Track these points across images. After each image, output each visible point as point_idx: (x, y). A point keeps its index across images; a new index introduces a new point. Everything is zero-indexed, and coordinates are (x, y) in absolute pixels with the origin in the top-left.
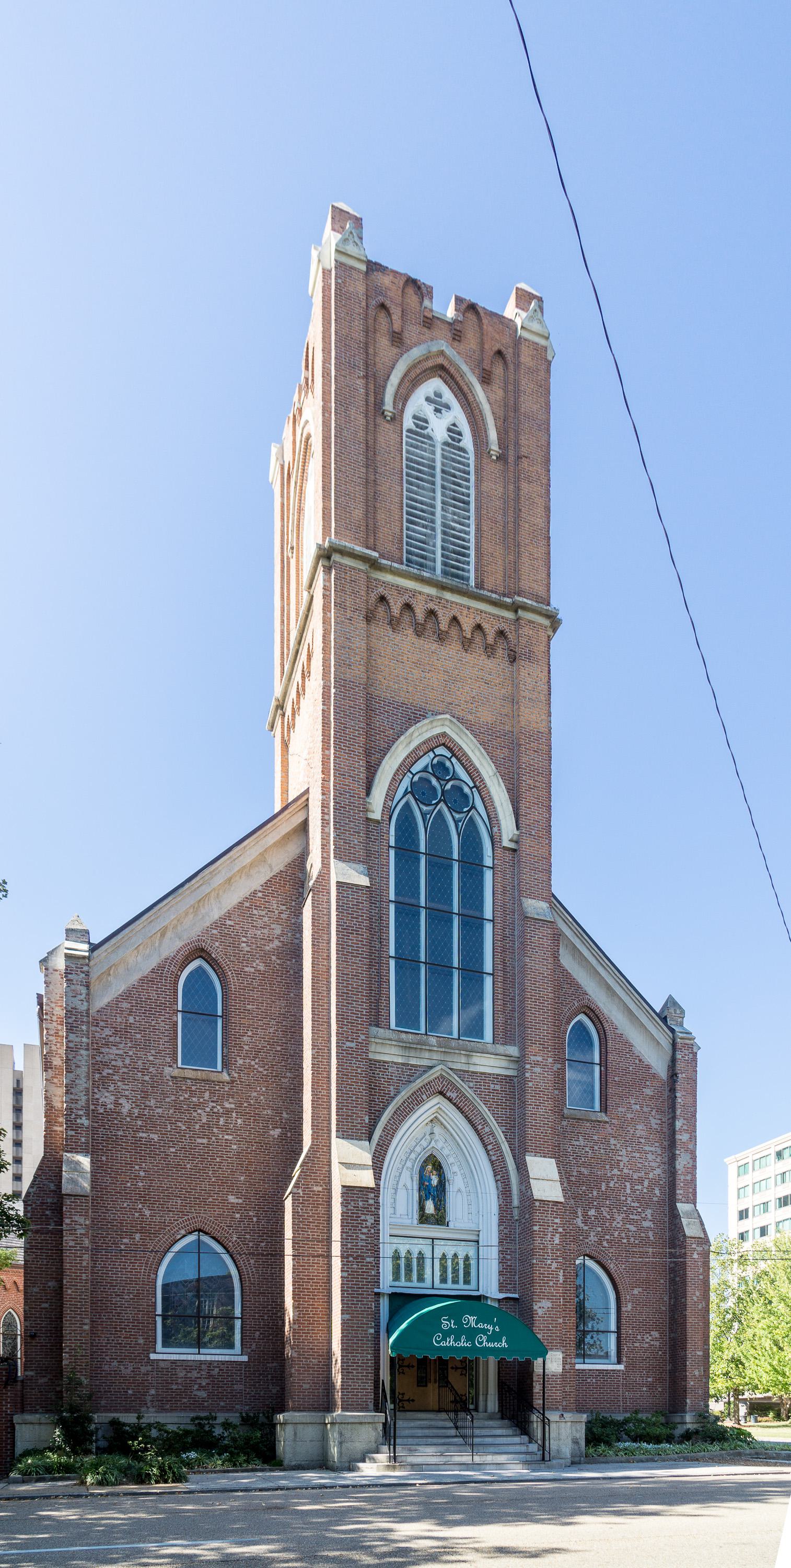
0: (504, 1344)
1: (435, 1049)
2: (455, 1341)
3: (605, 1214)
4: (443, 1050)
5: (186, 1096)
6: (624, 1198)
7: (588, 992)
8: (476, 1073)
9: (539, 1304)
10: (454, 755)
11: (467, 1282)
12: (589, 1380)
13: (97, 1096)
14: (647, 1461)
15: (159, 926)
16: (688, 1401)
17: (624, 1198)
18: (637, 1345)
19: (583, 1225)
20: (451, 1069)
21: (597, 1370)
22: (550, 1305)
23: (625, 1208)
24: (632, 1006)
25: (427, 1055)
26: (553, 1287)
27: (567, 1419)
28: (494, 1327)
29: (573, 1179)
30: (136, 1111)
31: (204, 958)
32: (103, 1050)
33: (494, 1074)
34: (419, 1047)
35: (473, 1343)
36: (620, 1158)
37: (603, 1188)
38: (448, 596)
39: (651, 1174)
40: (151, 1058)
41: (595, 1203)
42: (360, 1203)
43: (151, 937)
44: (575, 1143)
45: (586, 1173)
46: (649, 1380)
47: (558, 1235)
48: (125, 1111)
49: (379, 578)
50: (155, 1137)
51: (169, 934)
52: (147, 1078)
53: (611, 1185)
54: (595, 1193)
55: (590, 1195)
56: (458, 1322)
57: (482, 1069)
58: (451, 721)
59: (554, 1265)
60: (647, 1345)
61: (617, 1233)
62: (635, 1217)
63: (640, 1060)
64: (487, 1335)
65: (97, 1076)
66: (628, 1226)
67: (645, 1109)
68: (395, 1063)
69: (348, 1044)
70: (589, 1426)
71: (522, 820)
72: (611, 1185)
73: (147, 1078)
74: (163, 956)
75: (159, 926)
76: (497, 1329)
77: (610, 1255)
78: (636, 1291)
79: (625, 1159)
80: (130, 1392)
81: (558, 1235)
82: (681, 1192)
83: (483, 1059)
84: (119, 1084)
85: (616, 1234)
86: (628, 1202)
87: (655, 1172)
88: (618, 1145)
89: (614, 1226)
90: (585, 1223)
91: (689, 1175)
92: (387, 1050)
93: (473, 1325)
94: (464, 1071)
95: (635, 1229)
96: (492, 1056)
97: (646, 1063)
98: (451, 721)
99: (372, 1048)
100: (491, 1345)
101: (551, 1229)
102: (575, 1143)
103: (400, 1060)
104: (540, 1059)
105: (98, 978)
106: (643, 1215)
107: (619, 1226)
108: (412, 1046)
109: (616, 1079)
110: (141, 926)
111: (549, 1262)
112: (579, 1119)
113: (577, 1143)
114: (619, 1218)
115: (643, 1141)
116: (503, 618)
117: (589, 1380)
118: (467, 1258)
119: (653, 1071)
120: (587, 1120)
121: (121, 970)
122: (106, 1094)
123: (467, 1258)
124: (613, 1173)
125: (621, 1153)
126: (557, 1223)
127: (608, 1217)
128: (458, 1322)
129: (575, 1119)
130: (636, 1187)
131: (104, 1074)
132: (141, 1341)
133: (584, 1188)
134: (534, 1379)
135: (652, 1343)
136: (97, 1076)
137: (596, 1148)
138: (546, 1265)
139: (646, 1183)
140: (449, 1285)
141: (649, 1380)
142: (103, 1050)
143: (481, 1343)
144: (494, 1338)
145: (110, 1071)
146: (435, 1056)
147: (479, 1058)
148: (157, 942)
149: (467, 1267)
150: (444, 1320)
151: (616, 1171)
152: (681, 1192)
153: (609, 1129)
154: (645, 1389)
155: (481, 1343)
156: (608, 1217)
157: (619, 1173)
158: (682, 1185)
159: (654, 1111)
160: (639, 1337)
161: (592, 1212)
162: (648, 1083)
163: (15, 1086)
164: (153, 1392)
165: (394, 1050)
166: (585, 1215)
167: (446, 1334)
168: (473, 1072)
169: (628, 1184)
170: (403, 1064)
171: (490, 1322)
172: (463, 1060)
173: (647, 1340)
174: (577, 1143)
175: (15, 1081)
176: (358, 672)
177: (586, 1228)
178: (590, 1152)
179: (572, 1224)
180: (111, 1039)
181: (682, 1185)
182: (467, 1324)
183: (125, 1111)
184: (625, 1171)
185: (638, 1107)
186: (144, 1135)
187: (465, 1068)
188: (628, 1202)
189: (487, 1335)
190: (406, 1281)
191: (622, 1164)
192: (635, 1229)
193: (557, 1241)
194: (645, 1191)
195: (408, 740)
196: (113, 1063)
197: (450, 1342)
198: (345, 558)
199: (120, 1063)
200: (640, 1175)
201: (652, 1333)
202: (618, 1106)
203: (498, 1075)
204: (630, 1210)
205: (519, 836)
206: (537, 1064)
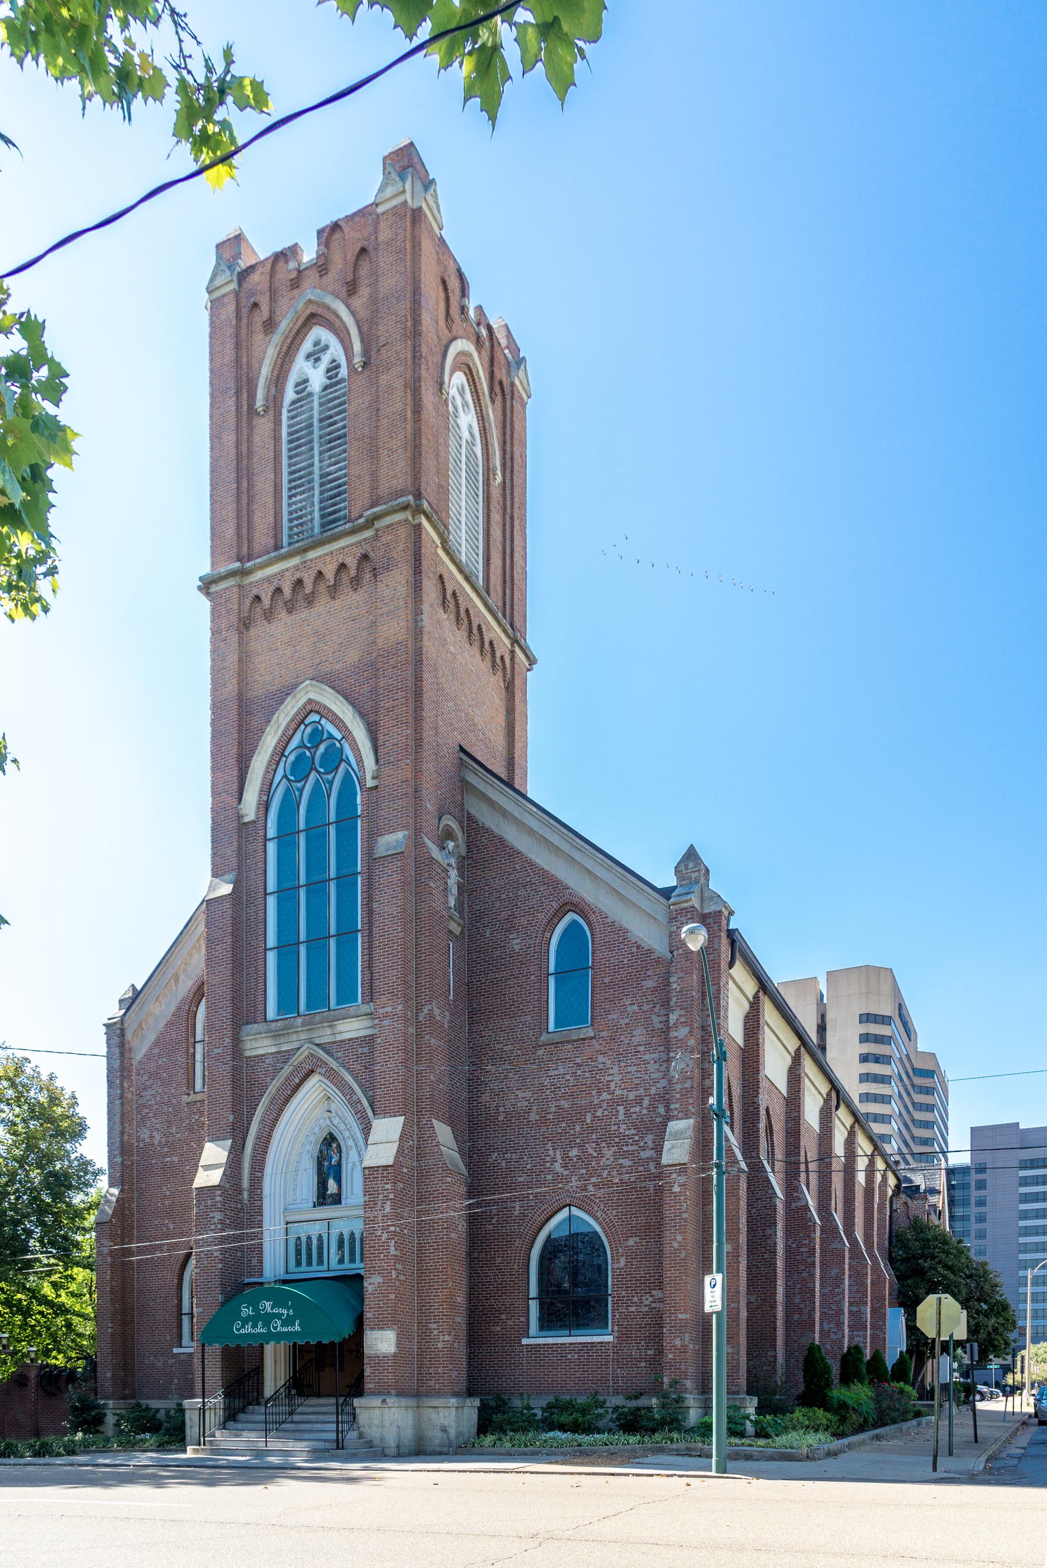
0: (297, 1328)
1: (300, 1029)
2: (252, 1327)
3: (591, 1151)
4: (307, 1028)
5: (197, 1117)
6: (616, 1127)
7: (569, 885)
8: (344, 1041)
9: (370, 1281)
10: (302, 722)
11: (320, 1262)
12: (569, 1356)
13: (139, 1134)
14: (533, 1454)
15: (171, 972)
16: (665, 1379)
17: (616, 1127)
18: (633, 1309)
19: (562, 1169)
20: (318, 1045)
21: (579, 1343)
22: (380, 1280)
23: (617, 1140)
24: (617, 884)
25: (294, 1037)
26: (384, 1259)
27: (390, 1405)
28: (288, 1311)
29: (550, 1116)
30: (163, 1140)
31: (574, 911)
32: (142, 1094)
33: (361, 1037)
34: (285, 1032)
35: (269, 1329)
36: (610, 1078)
37: (588, 1121)
38: (311, 555)
39: (654, 1088)
40: (173, 1091)
41: (578, 1141)
42: (209, 1202)
43: (166, 986)
44: (553, 1073)
45: (566, 1106)
46: (650, 1352)
47: (388, 1202)
48: (156, 1142)
49: (252, 580)
50: (175, 1159)
51: (182, 977)
52: (170, 1109)
53: (599, 1114)
54: (578, 1128)
55: (572, 1132)
56: (256, 1309)
57: (348, 1036)
58: (311, 685)
59: (385, 1236)
60: (647, 1309)
61: (606, 1172)
62: (631, 1148)
63: (638, 947)
64: (282, 1319)
65: (139, 1116)
66: (621, 1161)
67: (646, 1008)
68: (271, 1054)
69: (216, 1051)
70: (482, 1410)
71: (381, 750)
72: (599, 1114)
73: (170, 1109)
74: (179, 999)
75: (171, 972)
76: (291, 1312)
77: (597, 1200)
78: (631, 1242)
79: (617, 1078)
80: (161, 1382)
81: (388, 1202)
82: (677, 1106)
83: (346, 1025)
84: (153, 1119)
85: (605, 1173)
86: (622, 1131)
87: (658, 1085)
88: (609, 1062)
89: (602, 1164)
90: (565, 1166)
91: (689, 1081)
92: (321, 1032)
93: (269, 1310)
94: (333, 1043)
95: (630, 1163)
96: (354, 1019)
97: (646, 948)
98: (311, 685)
99: (248, 1045)
100: (285, 1329)
101: (381, 1197)
102: (553, 1073)
103: (273, 1050)
104: (389, 1009)
105: (133, 1035)
106: (642, 1144)
107: (608, 1163)
108: (279, 1033)
109: (606, 980)
110: (156, 981)
111: (379, 1233)
112: (558, 1043)
113: (556, 1072)
114: (609, 1153)
115: (641, 1049)
116: (365, 540)
117: (569, 1356)
118: (320, 1237)
119: (657, 955)
120: (568, 1042)
121: (151, 1021)
122: (145, 1131)
123: (320, 1237)
124: (601, 1098)
125: (611, 1072)
126: (388, 1190)
127: (595, 1154)
128: (256, 1309)
129: (552, 1044)
130: (632, 1110)
131: (144, 1114)
132: (168, 1338)
133: (564, 1125)
134: (365, 1361)
135: (653, 1305)
136: (139, 1116)
137: (579, 1072)
138: (376, 1236)
139: (646, 1102)
140: (304, 1267)
141: (650, 1352)
142: (142, 1094)
143: (275, 1328)
144: (288, 1322)
145: (147, 1111)
146: (303, 1036)
147: (342, 1026)
148: (174, 988)
149: (320, 1248)
150: (244, 1307)
151: (605, 1096)
152: (677, 1106)
153: (597, 1045)
154: (643, 1364)
155: (275, 1328)
156: (595, 1154)
157: (609, 1097)
158: (678, 1096)
159: (658, 1006)
160: (635, 1299)
161: (574, 1152)
162: (649, 973)
163: (820, 1022)
164: (176, 1381)
165: (267, 1042)
166: (565, 1156)
167: (245, 1322)
168: (341, 1041)
169: (621, 1109)
170: (277, 1053)
171: (284, 1306)
172: (328, 1031)
173: (647, 1302)
174: (556, 1072)
175: (820, 1017)
176: (231, 688)
177: (566, 1172)
178: (572, 1079)
179: (444, 1183)
180: (148, 1083)
181: (678, 1096)
182: (263, 1310)
183: (156, 1142)
184: (618, 1092)
185: (635, 1007)
186: (168, 1159)
187: (331, 1039)
188: (622, 1131)
189: (282, 1319)
190: (318, 1265)
191: (612, 1085)
192: (630, 1163)
193: (388, 1209)
194: (645, 1112)
195: (276, 727)
196: (149, 1103)
197: (248, 1329)
198: (219, 584)
199: (153, 1102)
200: (638, 1093)
201: (654, 1292)
202: (608, 1013)
203: (365, 1037)
204: (624, 1139)
205: (378, 770)
206: (386, 1016)
